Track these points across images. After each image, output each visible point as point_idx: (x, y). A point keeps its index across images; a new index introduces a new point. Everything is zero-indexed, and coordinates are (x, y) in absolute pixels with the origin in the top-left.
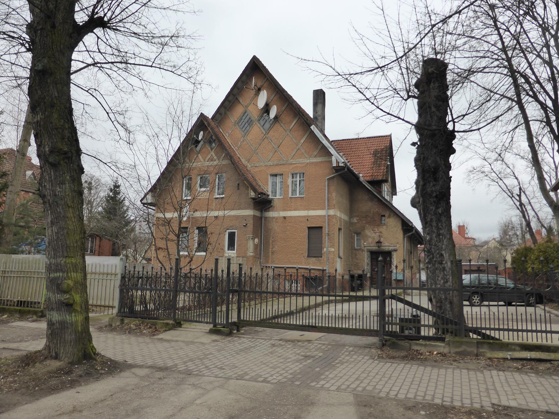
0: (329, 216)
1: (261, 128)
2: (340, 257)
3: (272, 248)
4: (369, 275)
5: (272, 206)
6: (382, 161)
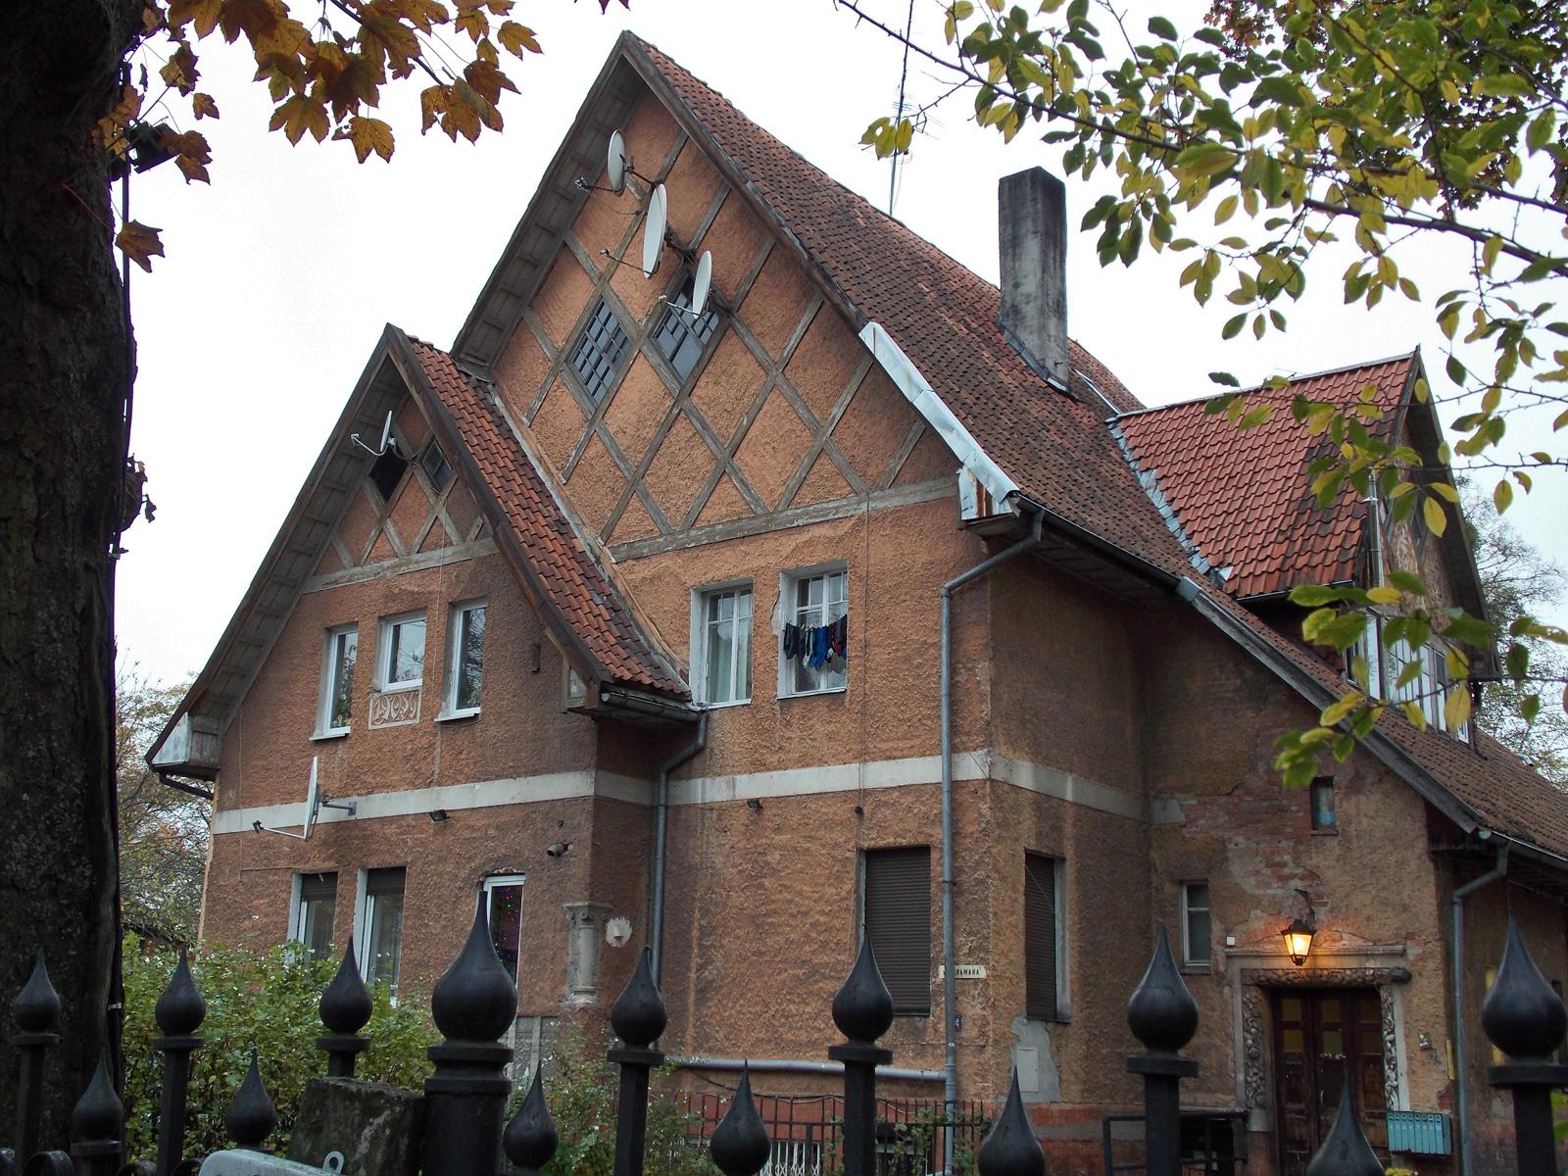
0: (955, 786)
1: (664, 370)
3: (701, 968)
5: (700, 751)
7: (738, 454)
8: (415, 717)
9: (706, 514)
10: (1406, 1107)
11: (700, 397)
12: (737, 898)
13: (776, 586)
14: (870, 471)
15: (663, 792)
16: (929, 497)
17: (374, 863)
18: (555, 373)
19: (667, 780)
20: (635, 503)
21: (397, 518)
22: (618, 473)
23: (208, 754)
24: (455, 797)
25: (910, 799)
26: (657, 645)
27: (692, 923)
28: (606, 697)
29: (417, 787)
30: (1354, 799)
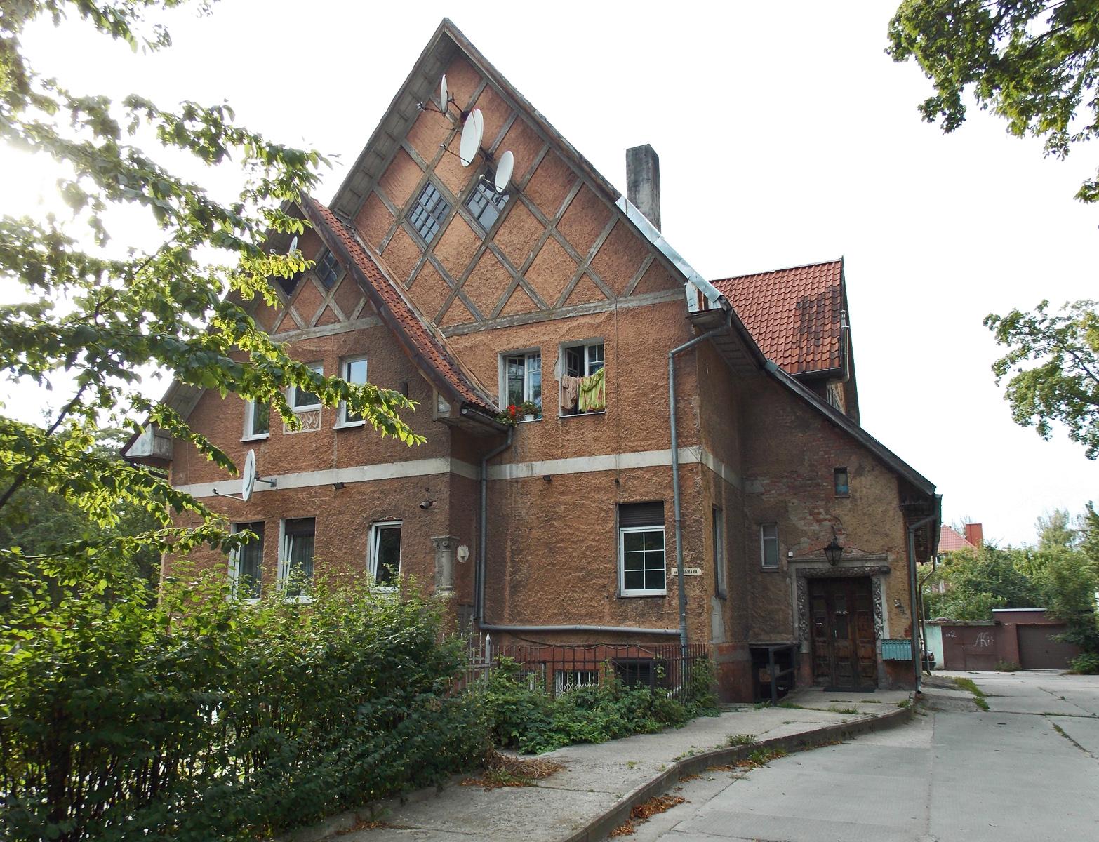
0: (680, 467)
1: (474, 225)
2: (718, 595)
3: (513, 574)
4: (805, 649)
5: (508, 448)
6: (824, 324)
7: (527, 274)
8: (317, 427)
9: (507, 309)
10: (887, 637)
11: (500, 241)
12: (536, 533)
13: (556, 352)
14: (616, 286)
15: (484, 472)
16: (656, 301)
17: (291, 515)
18: (398, 223)
19: (487, 465)
20: (457, 302)
21: (298, 305)
22: (445, 284)
23: (165, 449)
24: (349, 475)
25: (649, 474)
26: (476, 386)
27: (506, 548)
28: (465, 412)
29: (321, 469)
30: (858, 479)
